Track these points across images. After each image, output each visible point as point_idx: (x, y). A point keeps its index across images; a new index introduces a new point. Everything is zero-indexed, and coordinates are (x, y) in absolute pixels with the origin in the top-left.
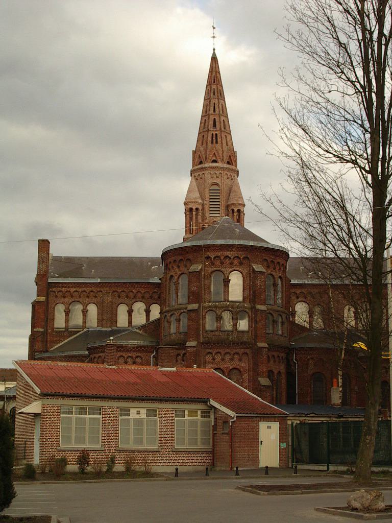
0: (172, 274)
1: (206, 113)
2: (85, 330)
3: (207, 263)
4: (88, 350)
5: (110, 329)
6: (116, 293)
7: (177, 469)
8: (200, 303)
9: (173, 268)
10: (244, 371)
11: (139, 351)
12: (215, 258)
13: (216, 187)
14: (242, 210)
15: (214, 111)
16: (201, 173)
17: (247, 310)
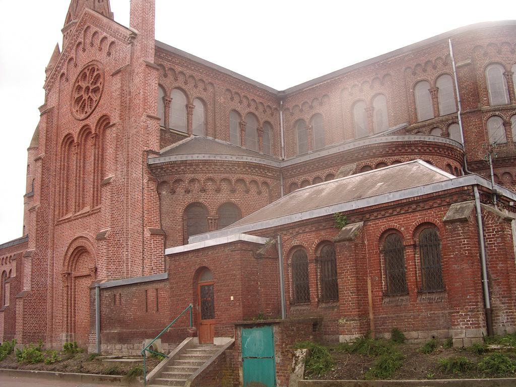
2: (192, 137)
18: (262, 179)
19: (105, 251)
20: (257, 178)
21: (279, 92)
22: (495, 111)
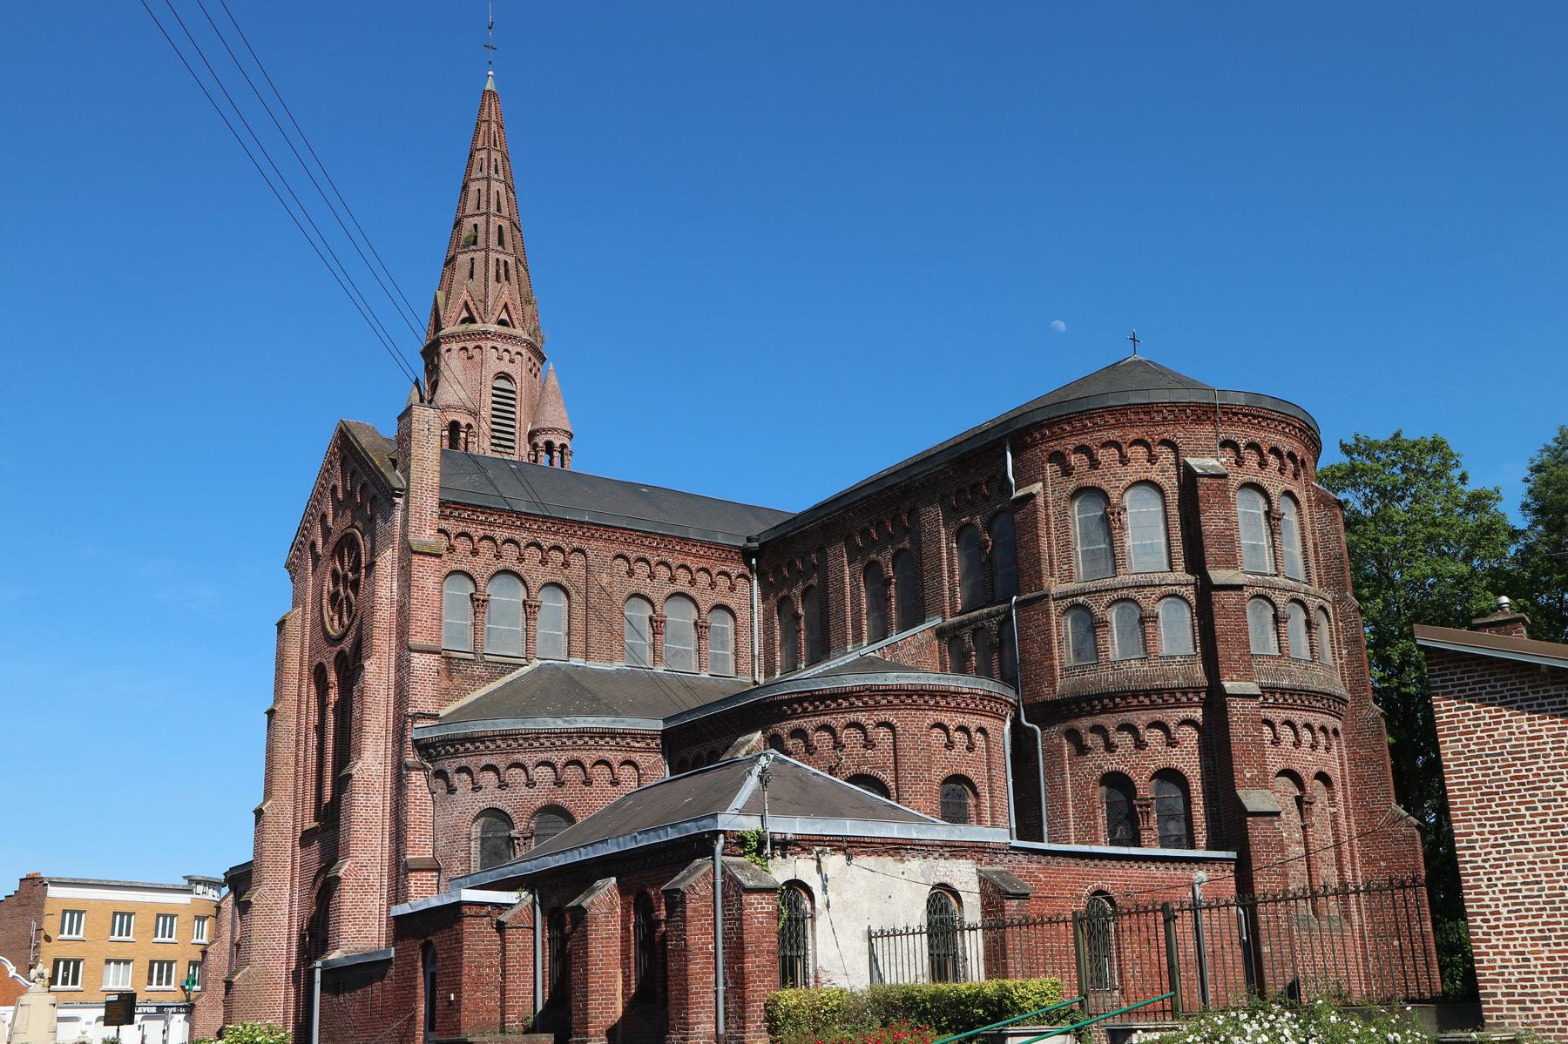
1: (478, 208)
2: (536, 663)
6: (620, 561)
13: (503, 384)
16: (470, 345)
18: (621, 756)
19: (1233, 978)
20: (608, 755)
21: (796, 518)
22: (1076, 596)
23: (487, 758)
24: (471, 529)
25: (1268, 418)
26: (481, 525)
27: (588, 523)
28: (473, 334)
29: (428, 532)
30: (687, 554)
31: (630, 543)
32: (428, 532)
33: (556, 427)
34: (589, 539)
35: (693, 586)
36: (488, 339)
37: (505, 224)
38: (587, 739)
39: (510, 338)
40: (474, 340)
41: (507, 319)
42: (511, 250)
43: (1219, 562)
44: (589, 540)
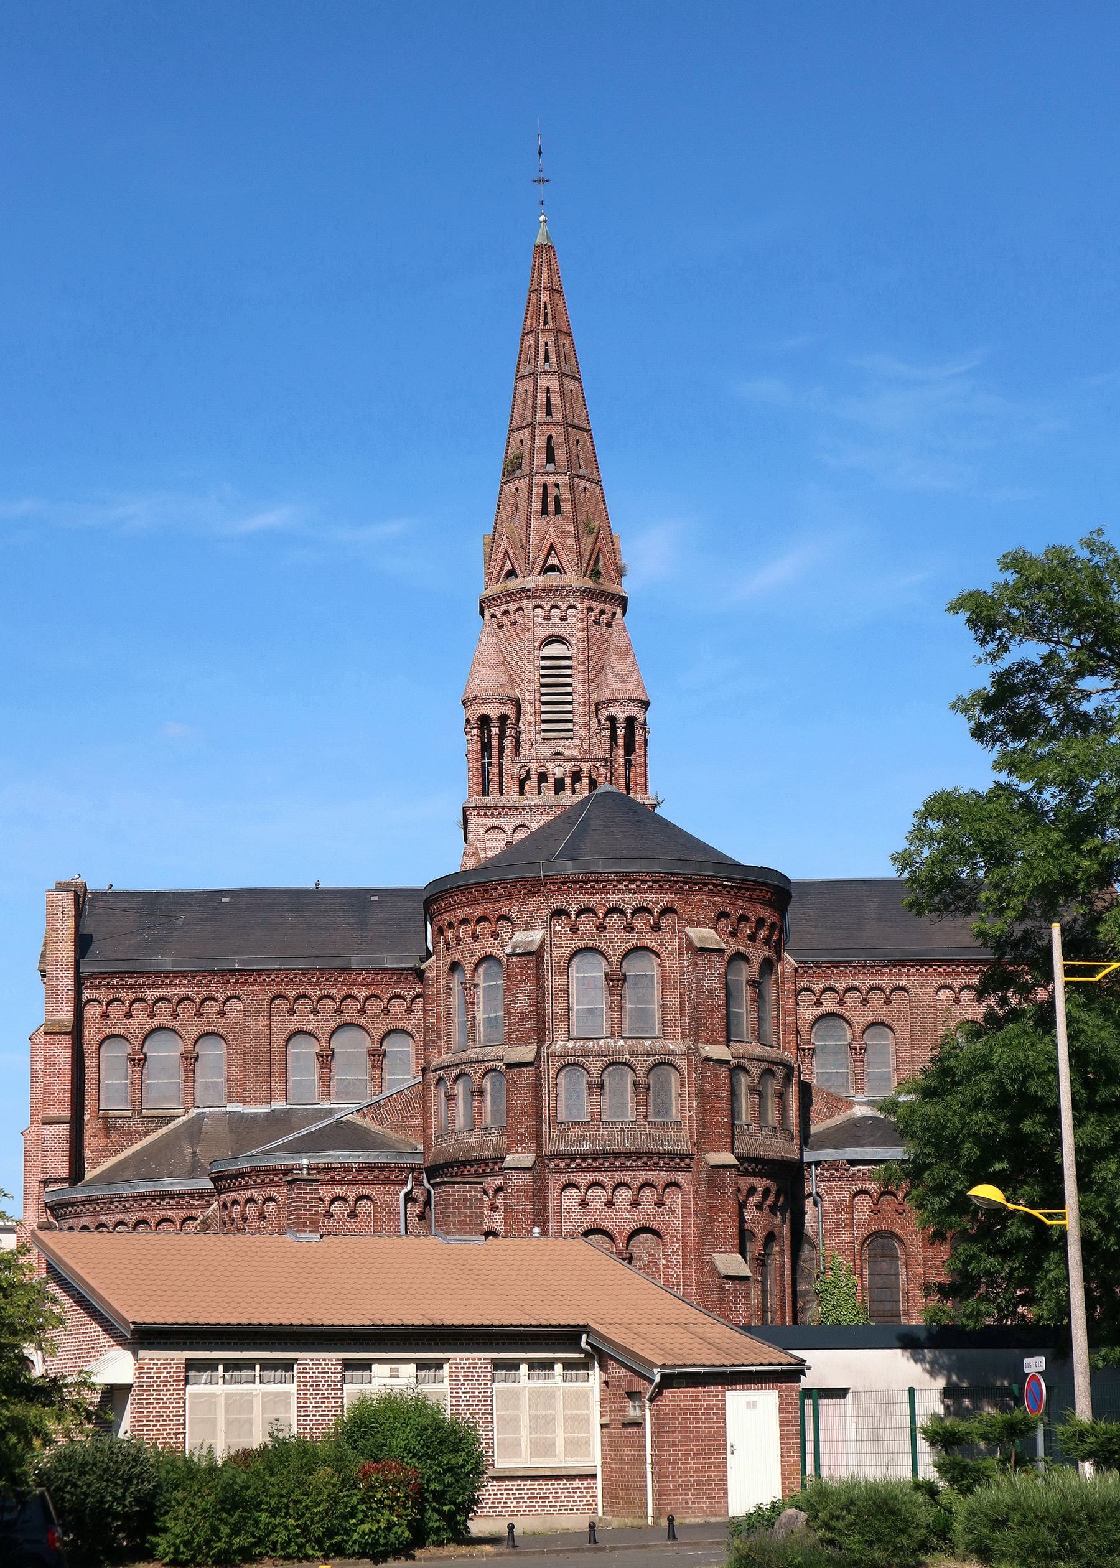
0: (457, 957)
2: (194, 1112)
3: (558, 928)
4: (213, 1180)
5: (264, 1109)
7: (511, 1527)
8: (540, 1042)
9: (458, 940)
10: (673, 1236)
11: (366, 1181)
12: (580, 913)
14: (641, 719)
15: (549, 412)
16: (512, 607)
17: (676, 1060)
23: (82, 1219)
24: (122, 995)
25: (602, 881)
26: (132, 989)
27: (238, 970)
28: (513, 593)
29: (65, 1009)
30: (353, 984)
31: (287, 982)
32: (65, 1009)
33: (618, 696)
34: (243, 984)
35: (362, 1015)
36: (528, 597)
37: (557, 432)
38: (149, 1201)
39: (557, 590)
40: (515, 600)
41: (558, 563)
42: (564, 466)
43: (521, 1038)
44: (244, 986)
